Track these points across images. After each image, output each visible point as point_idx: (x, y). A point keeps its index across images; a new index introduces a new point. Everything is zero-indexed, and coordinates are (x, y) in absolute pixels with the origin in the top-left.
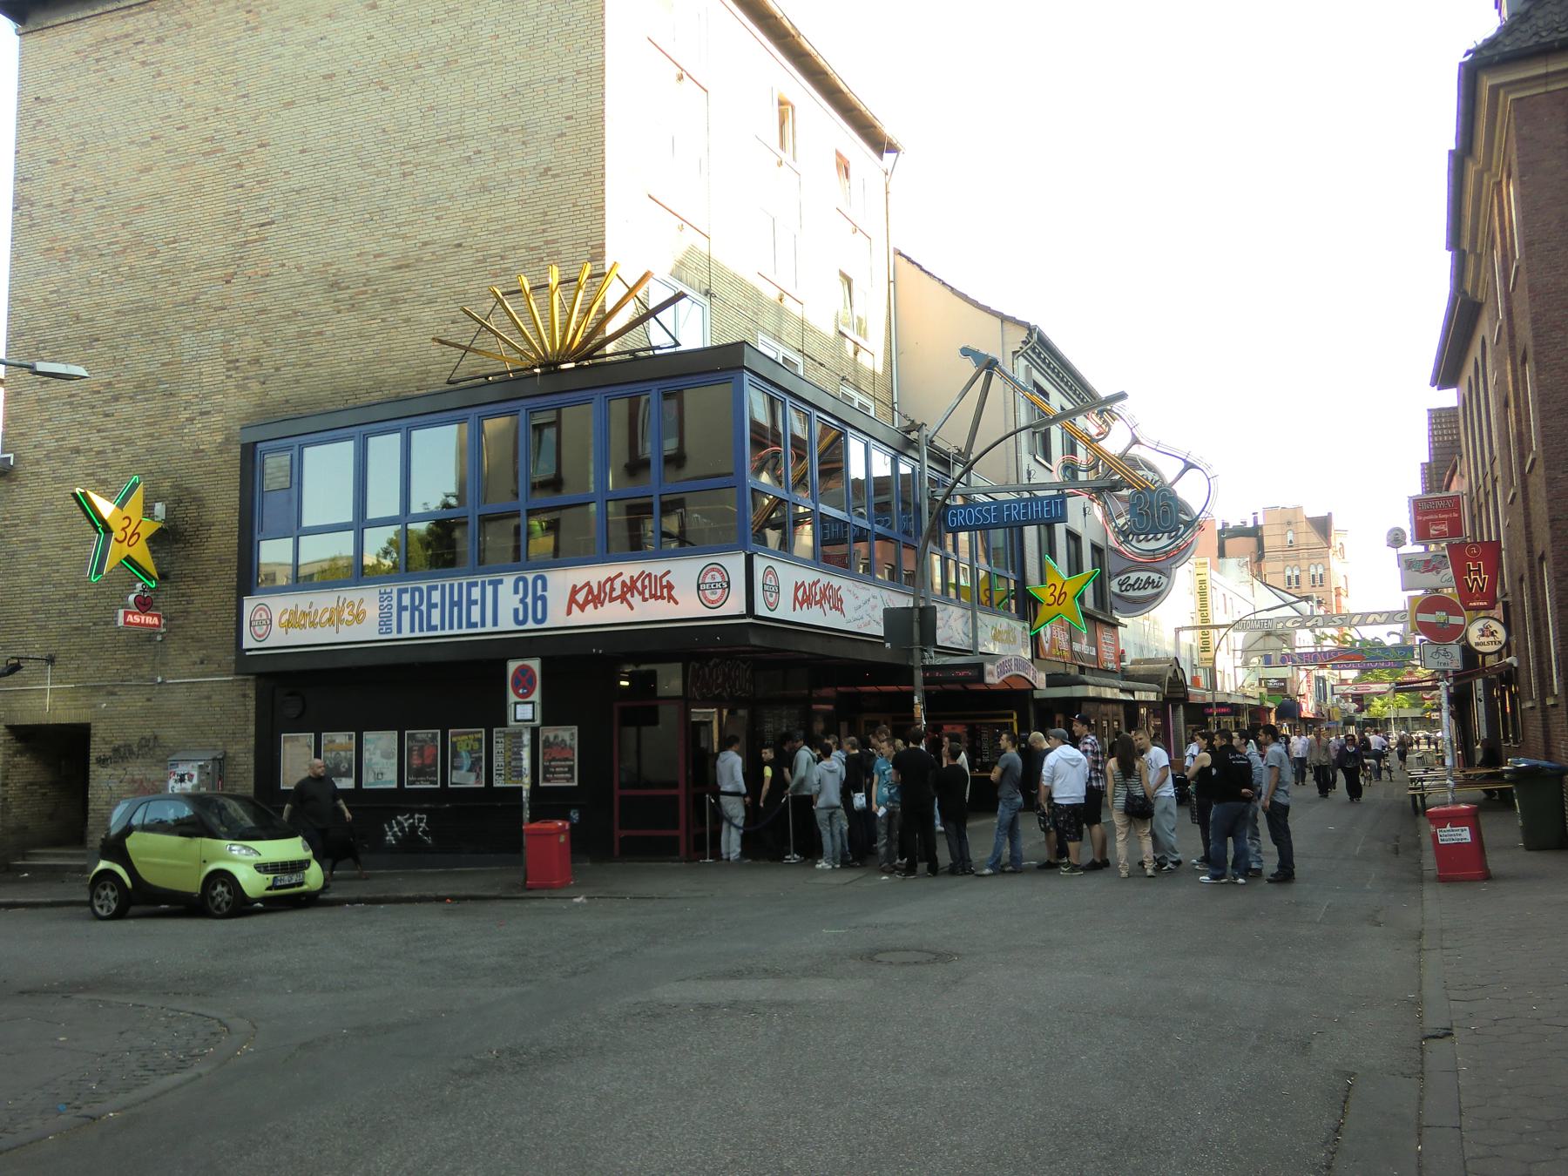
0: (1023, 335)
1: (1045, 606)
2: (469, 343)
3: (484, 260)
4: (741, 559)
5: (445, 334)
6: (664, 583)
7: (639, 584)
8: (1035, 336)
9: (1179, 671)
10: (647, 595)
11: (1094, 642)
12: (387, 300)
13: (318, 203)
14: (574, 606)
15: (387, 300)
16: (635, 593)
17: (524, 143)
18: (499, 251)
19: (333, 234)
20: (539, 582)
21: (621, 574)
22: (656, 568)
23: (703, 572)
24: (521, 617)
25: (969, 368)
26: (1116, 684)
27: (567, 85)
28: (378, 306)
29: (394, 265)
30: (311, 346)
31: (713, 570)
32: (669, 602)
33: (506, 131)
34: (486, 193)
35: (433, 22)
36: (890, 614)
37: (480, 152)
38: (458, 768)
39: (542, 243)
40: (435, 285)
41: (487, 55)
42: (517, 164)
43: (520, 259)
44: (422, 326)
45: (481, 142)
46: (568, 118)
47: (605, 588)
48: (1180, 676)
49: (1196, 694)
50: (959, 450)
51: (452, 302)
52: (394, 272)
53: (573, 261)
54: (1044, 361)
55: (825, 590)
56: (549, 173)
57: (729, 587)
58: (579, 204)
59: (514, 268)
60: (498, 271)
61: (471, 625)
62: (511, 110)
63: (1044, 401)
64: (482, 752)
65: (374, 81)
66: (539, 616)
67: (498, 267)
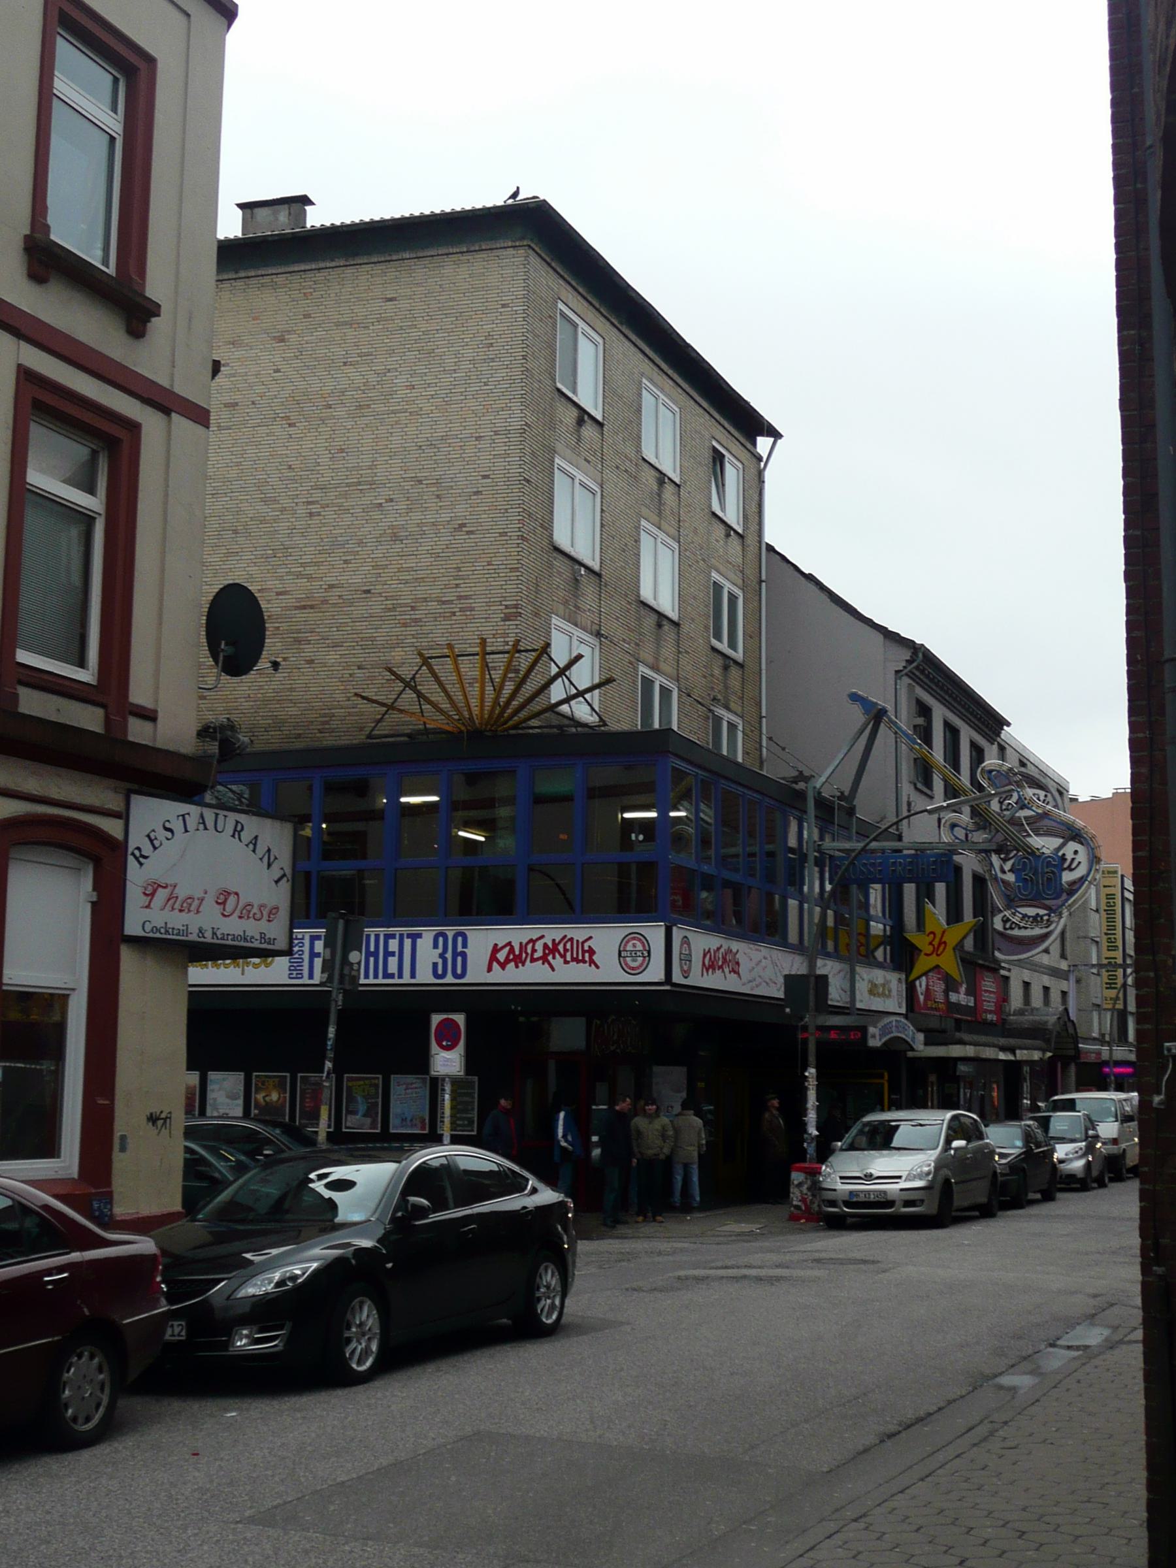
0: (907, 655)
1: (922, 957)
2: (391, 701)
3: (394, 609)
4: (661, 933)
5: (351, 679)
6: (586, 948)
7: (561, 948)
8: (920, 655)
9: (1069, 1024)
10: (569, 958)
11: (972, 991)
12: (289, 640)
13: (216, 533)
14: (495, 964)
15: (289, 640)
16: (557, 956)
17: (438, 496)
18: (409, 601)
19: (232, 566)
20: (460, 939)
21: (542, 937)
22: (578, 932)
23: (625, 940)
24: (440, 972)
25: (857, 716)
26: (996, 1042)
27: (484, 444)
28: (280, 644)
29: (298, 604)
30: (206, 679)
31: (634, 939)
32: (590, 965)
33: (420, 482)
34: (397, 542)
35: (345, 364)
36: (790, 980)
37: (391, 500)
38: (355, 1113)
39: (455, 598)
40: (341, 629)
41: (401, 404)
42: (430, 516)
43: (431, 611)
44: (326, 669)
45: (393, 491)
46: (485, 477)
47: (526, 949)
48: (1071, 1030)
49: (1089, 1052)
50: (842, 793)
51: (360, 647)
52: (297, 612)
53: (486, 618)
54: (927, 677)
55: (726, 954)
56: (464, 529)
57: (649, 955)
58: (494, 563)
59: (425, 620)
60: (408, 621)
61: (387, 975)
62: (426, 462)
63: (928, 752)
64: (378, 1098)
65: (280, 415)
66: (459, 971)
67: (408, 617)
